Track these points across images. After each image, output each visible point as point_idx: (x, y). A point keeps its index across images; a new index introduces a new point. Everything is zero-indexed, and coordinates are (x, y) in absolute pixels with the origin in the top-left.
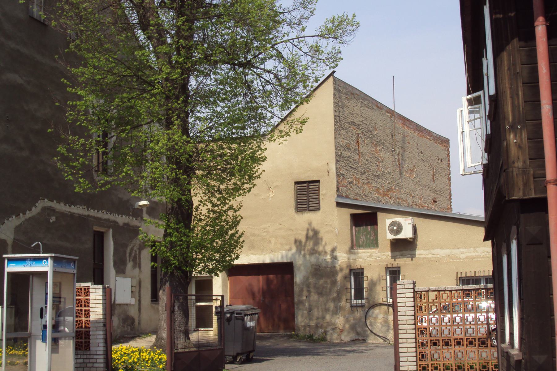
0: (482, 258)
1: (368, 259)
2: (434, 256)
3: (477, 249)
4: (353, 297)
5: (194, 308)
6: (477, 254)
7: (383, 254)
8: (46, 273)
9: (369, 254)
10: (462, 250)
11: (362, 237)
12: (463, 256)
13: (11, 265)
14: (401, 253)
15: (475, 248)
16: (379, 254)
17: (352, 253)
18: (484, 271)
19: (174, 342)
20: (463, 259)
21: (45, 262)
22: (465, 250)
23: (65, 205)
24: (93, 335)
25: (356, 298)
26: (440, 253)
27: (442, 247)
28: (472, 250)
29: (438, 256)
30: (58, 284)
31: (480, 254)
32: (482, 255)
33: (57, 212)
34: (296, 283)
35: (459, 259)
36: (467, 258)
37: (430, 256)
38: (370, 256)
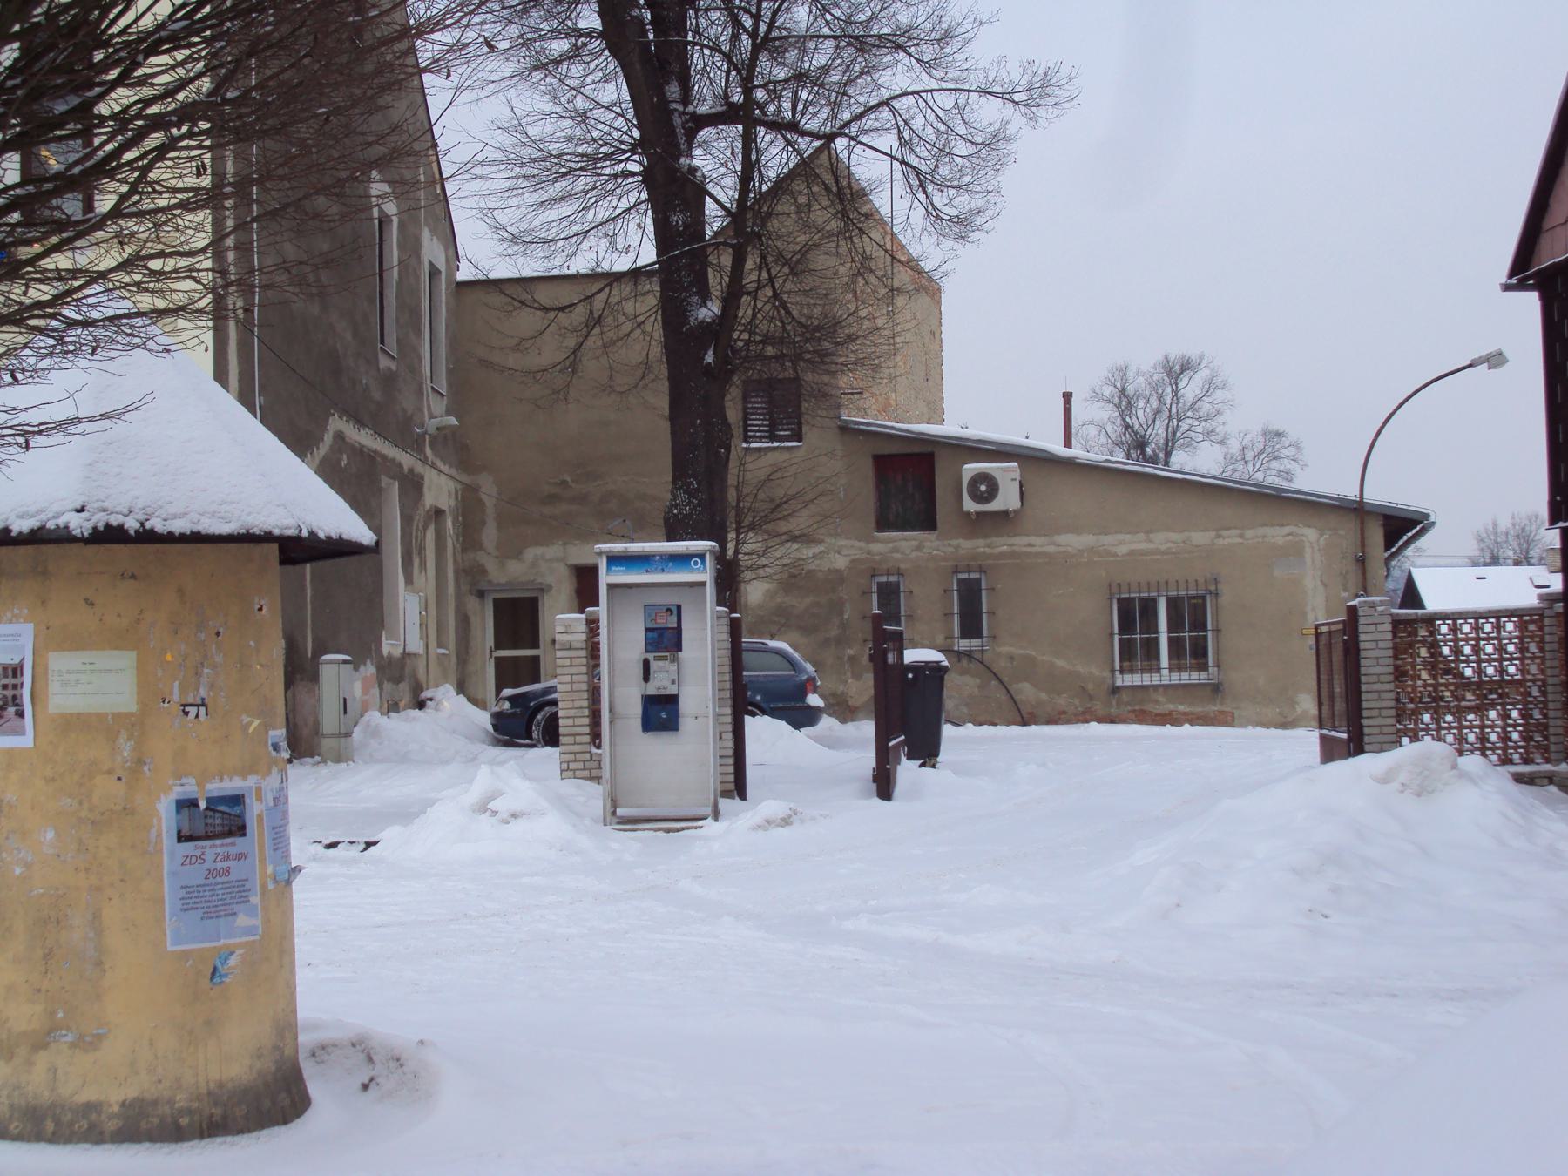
0: (1163, 553)
1: (914, 554)
2: (1061, 549)
3: (1151, 536)
4: (957, 633)
5: (493, 660)
6: (1152, 546)
7: (946, 542)
8: (703, 584)
9: (914, 543)
10: (1120, 537)
11: (893, 506)
12: (1123, 550)
13: (614, 568)
14: (988, 541)
15: (1148, 532)
16: (937, 543)
17: (812, 541)
18: (1167, 582)
19: (1320, 704)
20: (1123, 556)
21: (696, 563)
22: (1128, 537)
23: (341, 418)
24: (1368, 692)
25: (965, 634)
26: (1072, 542)
27: (1077, 530)
28: (1141, 536)
29: (1070, 550)
30: (674, 609)
31: (1160, 547)
32: (1163, 547)
33: (348, 443)
34: (746, 605)
35: (1115, 555)
36: (1132, 553)
37: (1051, 549)
38: (919, 548)
